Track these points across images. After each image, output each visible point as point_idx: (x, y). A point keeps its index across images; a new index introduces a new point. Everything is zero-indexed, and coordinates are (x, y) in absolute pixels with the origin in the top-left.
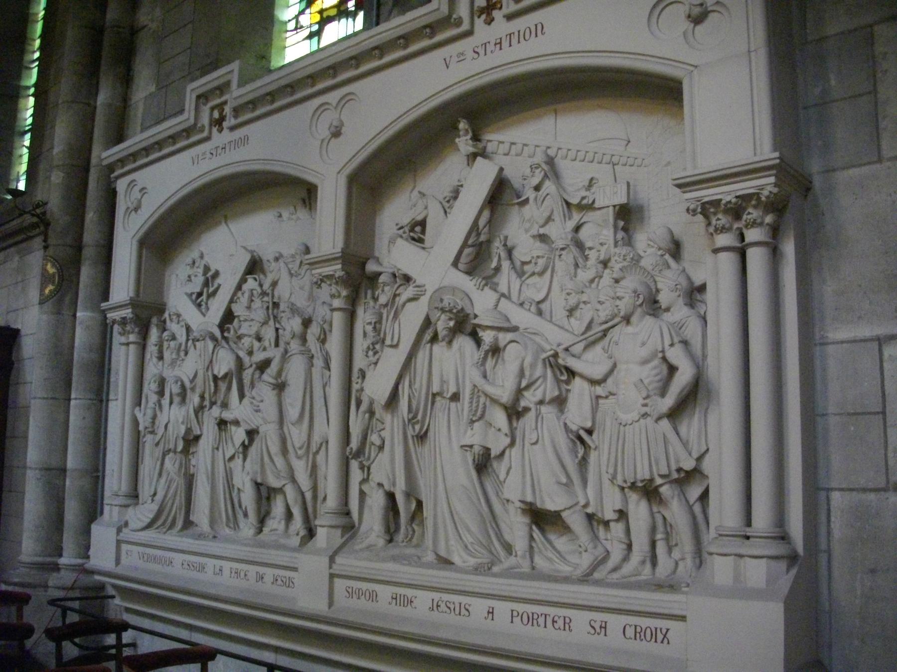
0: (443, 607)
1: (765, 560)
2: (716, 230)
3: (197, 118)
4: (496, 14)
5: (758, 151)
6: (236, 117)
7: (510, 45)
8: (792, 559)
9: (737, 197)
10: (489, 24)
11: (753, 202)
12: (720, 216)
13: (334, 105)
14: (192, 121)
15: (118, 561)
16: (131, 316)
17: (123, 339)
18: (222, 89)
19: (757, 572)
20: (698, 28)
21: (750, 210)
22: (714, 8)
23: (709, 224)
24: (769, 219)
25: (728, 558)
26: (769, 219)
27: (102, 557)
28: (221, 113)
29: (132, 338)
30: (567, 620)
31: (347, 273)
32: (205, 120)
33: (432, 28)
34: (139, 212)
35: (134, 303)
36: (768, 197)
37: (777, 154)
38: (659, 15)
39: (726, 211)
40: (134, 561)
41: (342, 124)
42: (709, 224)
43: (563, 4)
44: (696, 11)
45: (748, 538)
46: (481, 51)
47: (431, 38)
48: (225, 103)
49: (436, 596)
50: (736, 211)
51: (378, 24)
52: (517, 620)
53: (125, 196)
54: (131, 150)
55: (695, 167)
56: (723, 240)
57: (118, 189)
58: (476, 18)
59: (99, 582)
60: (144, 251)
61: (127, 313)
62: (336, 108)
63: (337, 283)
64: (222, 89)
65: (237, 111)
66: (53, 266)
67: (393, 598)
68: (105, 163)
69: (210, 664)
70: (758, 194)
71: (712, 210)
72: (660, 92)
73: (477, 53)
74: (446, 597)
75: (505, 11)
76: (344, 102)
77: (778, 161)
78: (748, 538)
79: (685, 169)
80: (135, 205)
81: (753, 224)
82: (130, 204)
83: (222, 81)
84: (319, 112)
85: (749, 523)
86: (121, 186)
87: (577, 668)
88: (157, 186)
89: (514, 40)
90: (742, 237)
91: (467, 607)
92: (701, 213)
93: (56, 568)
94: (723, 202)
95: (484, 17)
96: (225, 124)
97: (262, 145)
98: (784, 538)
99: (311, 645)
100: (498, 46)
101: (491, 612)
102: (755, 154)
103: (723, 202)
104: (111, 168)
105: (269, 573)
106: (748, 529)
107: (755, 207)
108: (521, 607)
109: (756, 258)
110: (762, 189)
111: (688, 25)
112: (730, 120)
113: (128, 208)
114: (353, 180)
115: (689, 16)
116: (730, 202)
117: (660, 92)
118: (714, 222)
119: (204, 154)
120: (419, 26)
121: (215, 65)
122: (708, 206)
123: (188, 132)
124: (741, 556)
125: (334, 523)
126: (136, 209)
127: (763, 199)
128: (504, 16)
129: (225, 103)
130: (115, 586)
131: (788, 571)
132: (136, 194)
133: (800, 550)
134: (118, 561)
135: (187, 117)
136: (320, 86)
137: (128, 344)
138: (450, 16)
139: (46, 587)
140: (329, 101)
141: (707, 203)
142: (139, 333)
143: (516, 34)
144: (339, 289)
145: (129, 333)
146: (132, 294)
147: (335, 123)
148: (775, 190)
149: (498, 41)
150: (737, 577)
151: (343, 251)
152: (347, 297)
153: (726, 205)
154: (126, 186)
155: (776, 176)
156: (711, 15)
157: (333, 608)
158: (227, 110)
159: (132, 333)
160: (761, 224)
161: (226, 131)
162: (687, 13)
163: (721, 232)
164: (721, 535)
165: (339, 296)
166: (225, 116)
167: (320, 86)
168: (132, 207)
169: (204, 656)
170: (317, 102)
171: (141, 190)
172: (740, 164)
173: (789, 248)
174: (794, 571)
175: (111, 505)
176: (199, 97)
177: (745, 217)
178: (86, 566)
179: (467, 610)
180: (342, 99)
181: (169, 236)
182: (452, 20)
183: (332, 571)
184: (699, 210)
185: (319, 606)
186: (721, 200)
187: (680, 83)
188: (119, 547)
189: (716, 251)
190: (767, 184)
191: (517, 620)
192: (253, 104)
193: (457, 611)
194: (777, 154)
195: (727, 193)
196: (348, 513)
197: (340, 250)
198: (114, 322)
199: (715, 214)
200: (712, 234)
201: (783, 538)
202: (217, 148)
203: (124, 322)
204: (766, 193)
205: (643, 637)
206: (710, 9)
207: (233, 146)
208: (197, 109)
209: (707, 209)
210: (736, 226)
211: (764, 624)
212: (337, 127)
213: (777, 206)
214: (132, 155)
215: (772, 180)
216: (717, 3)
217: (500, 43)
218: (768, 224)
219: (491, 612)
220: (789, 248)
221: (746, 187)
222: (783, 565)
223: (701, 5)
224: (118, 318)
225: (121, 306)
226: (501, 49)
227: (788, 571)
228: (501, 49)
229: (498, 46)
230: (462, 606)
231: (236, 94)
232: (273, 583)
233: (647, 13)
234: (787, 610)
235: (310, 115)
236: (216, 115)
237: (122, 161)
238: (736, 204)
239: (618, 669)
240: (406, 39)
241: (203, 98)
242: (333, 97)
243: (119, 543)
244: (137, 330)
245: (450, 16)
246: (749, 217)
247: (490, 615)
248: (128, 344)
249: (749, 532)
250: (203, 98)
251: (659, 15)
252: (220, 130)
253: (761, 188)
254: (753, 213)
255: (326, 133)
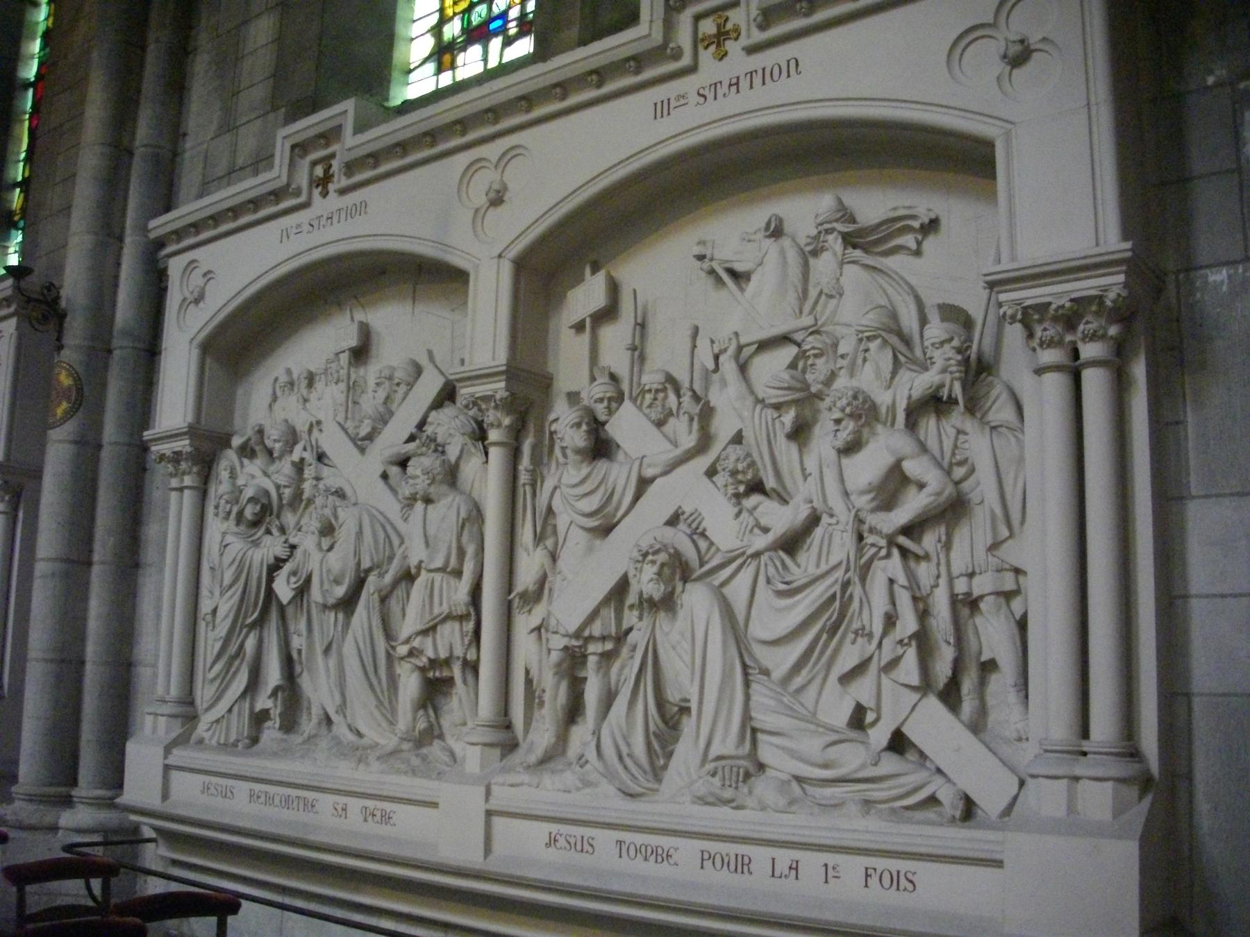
0: (562, 842)
1: (1109, 784)
2: (1041, 344)
3: (290, 175)
4: (730, 45)
5: (1102, 242)
6: (762, 27)
7: (751, 87)
8: (1145, 783)
9: (1072, 300)
10: (721, 59)
11: (1094, 308)
12: (1046, 324)
13: (494, 159)
14: (284, 179)
15: (165, 796)
16: (189, 449)
17: (174, 483)
18: (330, 136)
19: (1098, 799)
20: (1015, 72)
21: (1089, 318)
22: (1039, 46)
23: (1031, 335)
24: (1113, 331)
25: (1059, 781)
26: (1113, 331)
27: (141, 786)
28: (327, 171)
29: (188, 480)
30: (746, 860)
31: (513, 394)
32: (302, 179)
33: (638, 61)
34: (201, 304)
35: (192, 431)
36: (1114, 301)
37: (1128, 245)
38: (964, 50)
39: (1055, 319)
40: (190, 796)
41: (505, 188)
42: (1031, 335)
43: (917, 4)
44: (1015, 49)
45: (1085, 754)
46: (315, 223)
47: (807, 15)
48: (333, 156)
49: (554, 828)
50: (1070, 319)
51: (168, 209)
52: (873, 881)
53: (181, 282)
54: (400, 137)
55: (1013, 258)
56: (1050, 356)
57: (170, 272)
58: (701, 48)
59: (131, 822)
60: (208, 361)
61: (183, 445)
62: (496, 167)
63: (496, 407)
64: (330, 136)
65: (350, 168)
66: (70, 375)
67: (790, 868)
68: (152, 235)
69: (230, 919)
70: (1101, 297)
71: (1036, 317)
72: (964, 160)
73: (704, 97)
74: (214, 780)
75: (744, 41)
76: (505, 160)
77: (1129, 254)
78: (1085, 754)
79: (999, 261)
80: (196, 294)
81: (1092, 337)
82: (187, 295)
83: (329, 125)
84: (470, 173)
85: (1085, 733)
86: (175, 267)
87: (823, 931)
88: (229, 270)
89: (757, 80)
90: (1075, 354)
91: (910, 876)
92: (1020, 321)
93: (67, 802)
94: (1054, 306)
95: (713, 48)
96: (331, 187)
97: (389, 215)
98: (1133, 754)
99: (321, 882)
100: (734, 89)
101: (794, 867)
102: (1097, 245)
103: (1054, 306)
104: (160, 243)
105: (355, 804)
106: (1084, 743)
107: (1098, 314)
108: (881, 863)
109: (1095, 383)
110: (1106, 291)
111: (1000, 67)
112: (1059, 197)
113: (185, 299)
114: (520, 265)
115: (1005, 56)
116: (1063, 307)
117: (964, 160)
118: (1038, 333)
119: (298, 226)
120: (548, 83)
121: (314, 105)
122: (1030, 311)
123: (277, 195)
124: (1077, 779)
125: (487, 739)
126: (197, 301)
127: (1109, 303)
128: (743, 49)
129: (333, 156)
130: (156, 829)
131: (1140, 799)
132: (196, 279)
133: (1154, 766)
134: (165, 796)
135: (276, 175)
136: (472, 136)
137: (181, 490)
138: (664, 46)
139: (54, 828)
140: (522, 143)
141: (1029, 307)
142: (198, 474)
143: (760, 72)
144: (499, 415)
145: (184, 473)
146: (190, 418)
147: (496, 186)
148: (1124, 293)
149: (734, 81)
150: (1071, 808)
151: (508, 365)
152: (509, 427)
153: (1056, 310)
154: (461, 170)
155: (1126, 273)
156: (1035, 55)
157: (491, 857)
158: (336, 165)
159: (189, 473)
160: (1104, 337)
161: (332, 195)
162: (1002, 50)
163: (1049, 346)
164: (1046, 751)
165: (499, 426)
166: (332, 176)
167: (472, 136)
168: (190, 298)
169: (224, 906)
170: (463, 159)
171: (205, 275)
172: (1077, 255)
173: (1139, 370)
174: (1148, 799)
175: (156, 715)
176: (293, 147)
177: (1081, 327)
178: (118, 800)
179: (911, 882)
180: (472, 164)
181: (243, 341)
182: (669, 51)
183: (489, 807)
184: (1019, 316)
185: (472, 857)
186: (1050, 304)
187: (989, 145)
188: (177, 777)
189: (1040, 371)
190: (1113, 284)
191: (708, 864)
192: (375, 158)
193: (579, 848)
194: (1128, 245)
195: (1058, 293)
196: (509, 727)
197: (504, 362)
198: (162, 457)
199: (1040, 321)
200: (1034, 350)
201: (1132, 755)
202: (319, 217)
203: (177, 457)
204: (1112, 295)
205: (726, 861)
206: (1032, 47)
207: (343, 216)
208: (292, 165)
209: (1029, 317)
210: (1069, 338)
211: (1111, 870)
212: (498, 192)
213: (1124, 314)
214: (176, 232)
215: (1121, 278)
216: (1044, 39)
217: (737, 84)
218: (1111, 337)
219: (794, 867)
220: (1139, 370)
221: (1086, 286)
222: (1133, 792)
223: (1022, 41)
224: (168, 453)
225: (176, 435)
226: (738, 91)
227: (1140, 799)
228: (738, 91)
229: (734, 89)
230: (902, 874)
231: (351, 143)
232: (548, 845)
233: (946, 52)
234: (1141, 847)
235: (457, 180)
236: (319, 171)
237: (179, 234)
238: (1071, 309)
239: (905, 933)
240: (600, 75)
241: (300, 148)
242: (491, 151)
243: (167, 768)
244: (195, 469)
245: (288, 185)
246: (1090, 326)
247: (793, 872)
248: (181, 490)
249: (1086, 746)
250: (300, 148)
251: (964, 50)
252: (325, 194)
253: (1105, 289)
254: (1089, 324)
255: (482, 200)
